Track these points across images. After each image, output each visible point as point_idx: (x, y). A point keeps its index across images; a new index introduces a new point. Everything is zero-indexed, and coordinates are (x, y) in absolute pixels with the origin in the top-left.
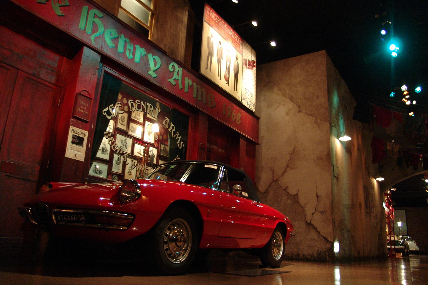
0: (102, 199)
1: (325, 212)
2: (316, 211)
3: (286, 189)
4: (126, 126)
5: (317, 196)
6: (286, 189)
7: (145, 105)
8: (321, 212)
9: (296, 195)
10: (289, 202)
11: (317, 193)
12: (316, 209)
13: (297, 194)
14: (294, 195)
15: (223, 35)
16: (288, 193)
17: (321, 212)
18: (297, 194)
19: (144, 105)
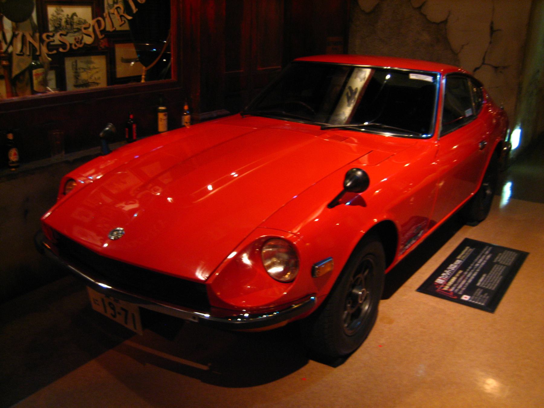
0: (207, 316)
1: (504, 68)
2: (483, 63)
3: (420, 8)
4: (76, 58)
5: (492, 31)
6: (420, 8)
7: (35, 40)
8: (496, 68)
9: (442, 22)
10: (426, 37)
11: (492, 23)
12: (484, 59)
13: (445, 22)
14: (438, 24)
15: (215, 115)
16: (425, 16)
17: (496, 68)
18: (445, 22)
19: (31, 40)
